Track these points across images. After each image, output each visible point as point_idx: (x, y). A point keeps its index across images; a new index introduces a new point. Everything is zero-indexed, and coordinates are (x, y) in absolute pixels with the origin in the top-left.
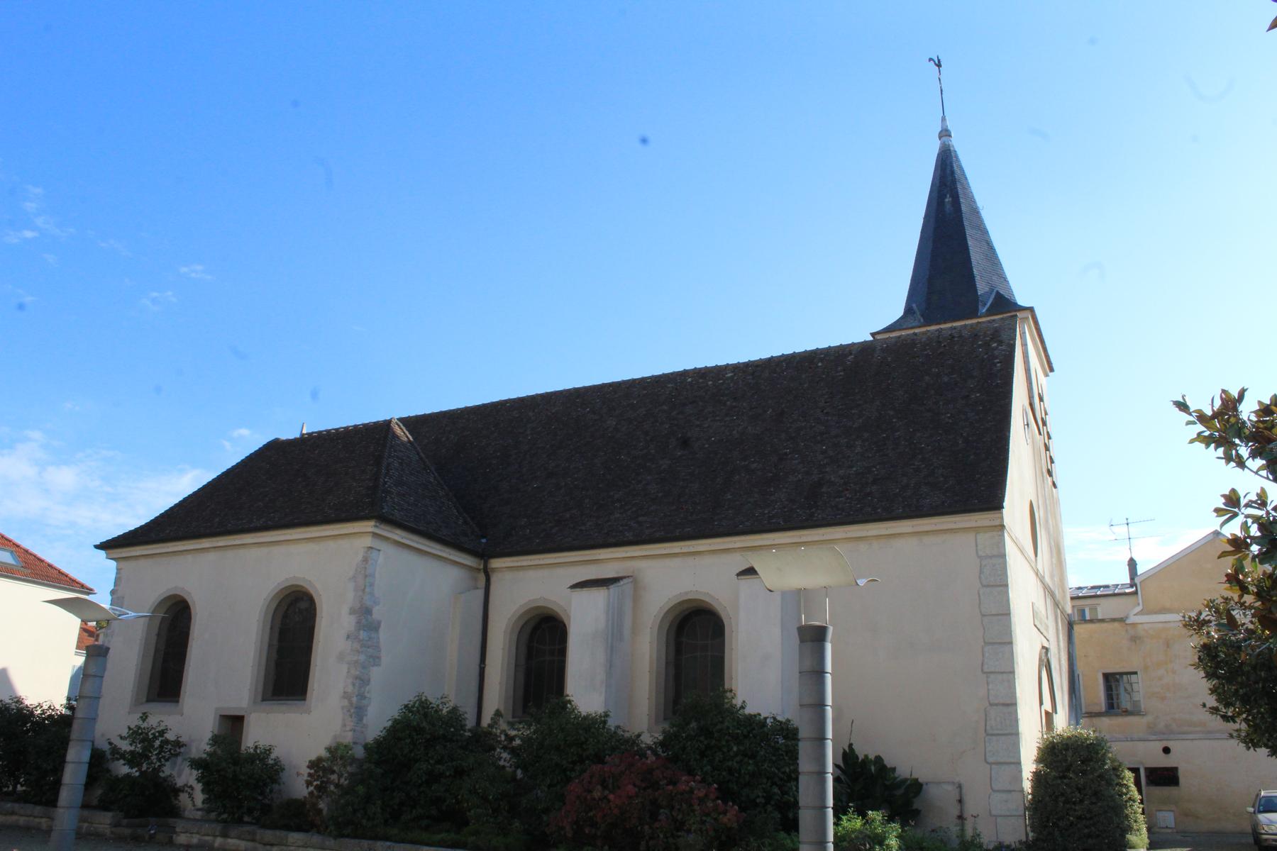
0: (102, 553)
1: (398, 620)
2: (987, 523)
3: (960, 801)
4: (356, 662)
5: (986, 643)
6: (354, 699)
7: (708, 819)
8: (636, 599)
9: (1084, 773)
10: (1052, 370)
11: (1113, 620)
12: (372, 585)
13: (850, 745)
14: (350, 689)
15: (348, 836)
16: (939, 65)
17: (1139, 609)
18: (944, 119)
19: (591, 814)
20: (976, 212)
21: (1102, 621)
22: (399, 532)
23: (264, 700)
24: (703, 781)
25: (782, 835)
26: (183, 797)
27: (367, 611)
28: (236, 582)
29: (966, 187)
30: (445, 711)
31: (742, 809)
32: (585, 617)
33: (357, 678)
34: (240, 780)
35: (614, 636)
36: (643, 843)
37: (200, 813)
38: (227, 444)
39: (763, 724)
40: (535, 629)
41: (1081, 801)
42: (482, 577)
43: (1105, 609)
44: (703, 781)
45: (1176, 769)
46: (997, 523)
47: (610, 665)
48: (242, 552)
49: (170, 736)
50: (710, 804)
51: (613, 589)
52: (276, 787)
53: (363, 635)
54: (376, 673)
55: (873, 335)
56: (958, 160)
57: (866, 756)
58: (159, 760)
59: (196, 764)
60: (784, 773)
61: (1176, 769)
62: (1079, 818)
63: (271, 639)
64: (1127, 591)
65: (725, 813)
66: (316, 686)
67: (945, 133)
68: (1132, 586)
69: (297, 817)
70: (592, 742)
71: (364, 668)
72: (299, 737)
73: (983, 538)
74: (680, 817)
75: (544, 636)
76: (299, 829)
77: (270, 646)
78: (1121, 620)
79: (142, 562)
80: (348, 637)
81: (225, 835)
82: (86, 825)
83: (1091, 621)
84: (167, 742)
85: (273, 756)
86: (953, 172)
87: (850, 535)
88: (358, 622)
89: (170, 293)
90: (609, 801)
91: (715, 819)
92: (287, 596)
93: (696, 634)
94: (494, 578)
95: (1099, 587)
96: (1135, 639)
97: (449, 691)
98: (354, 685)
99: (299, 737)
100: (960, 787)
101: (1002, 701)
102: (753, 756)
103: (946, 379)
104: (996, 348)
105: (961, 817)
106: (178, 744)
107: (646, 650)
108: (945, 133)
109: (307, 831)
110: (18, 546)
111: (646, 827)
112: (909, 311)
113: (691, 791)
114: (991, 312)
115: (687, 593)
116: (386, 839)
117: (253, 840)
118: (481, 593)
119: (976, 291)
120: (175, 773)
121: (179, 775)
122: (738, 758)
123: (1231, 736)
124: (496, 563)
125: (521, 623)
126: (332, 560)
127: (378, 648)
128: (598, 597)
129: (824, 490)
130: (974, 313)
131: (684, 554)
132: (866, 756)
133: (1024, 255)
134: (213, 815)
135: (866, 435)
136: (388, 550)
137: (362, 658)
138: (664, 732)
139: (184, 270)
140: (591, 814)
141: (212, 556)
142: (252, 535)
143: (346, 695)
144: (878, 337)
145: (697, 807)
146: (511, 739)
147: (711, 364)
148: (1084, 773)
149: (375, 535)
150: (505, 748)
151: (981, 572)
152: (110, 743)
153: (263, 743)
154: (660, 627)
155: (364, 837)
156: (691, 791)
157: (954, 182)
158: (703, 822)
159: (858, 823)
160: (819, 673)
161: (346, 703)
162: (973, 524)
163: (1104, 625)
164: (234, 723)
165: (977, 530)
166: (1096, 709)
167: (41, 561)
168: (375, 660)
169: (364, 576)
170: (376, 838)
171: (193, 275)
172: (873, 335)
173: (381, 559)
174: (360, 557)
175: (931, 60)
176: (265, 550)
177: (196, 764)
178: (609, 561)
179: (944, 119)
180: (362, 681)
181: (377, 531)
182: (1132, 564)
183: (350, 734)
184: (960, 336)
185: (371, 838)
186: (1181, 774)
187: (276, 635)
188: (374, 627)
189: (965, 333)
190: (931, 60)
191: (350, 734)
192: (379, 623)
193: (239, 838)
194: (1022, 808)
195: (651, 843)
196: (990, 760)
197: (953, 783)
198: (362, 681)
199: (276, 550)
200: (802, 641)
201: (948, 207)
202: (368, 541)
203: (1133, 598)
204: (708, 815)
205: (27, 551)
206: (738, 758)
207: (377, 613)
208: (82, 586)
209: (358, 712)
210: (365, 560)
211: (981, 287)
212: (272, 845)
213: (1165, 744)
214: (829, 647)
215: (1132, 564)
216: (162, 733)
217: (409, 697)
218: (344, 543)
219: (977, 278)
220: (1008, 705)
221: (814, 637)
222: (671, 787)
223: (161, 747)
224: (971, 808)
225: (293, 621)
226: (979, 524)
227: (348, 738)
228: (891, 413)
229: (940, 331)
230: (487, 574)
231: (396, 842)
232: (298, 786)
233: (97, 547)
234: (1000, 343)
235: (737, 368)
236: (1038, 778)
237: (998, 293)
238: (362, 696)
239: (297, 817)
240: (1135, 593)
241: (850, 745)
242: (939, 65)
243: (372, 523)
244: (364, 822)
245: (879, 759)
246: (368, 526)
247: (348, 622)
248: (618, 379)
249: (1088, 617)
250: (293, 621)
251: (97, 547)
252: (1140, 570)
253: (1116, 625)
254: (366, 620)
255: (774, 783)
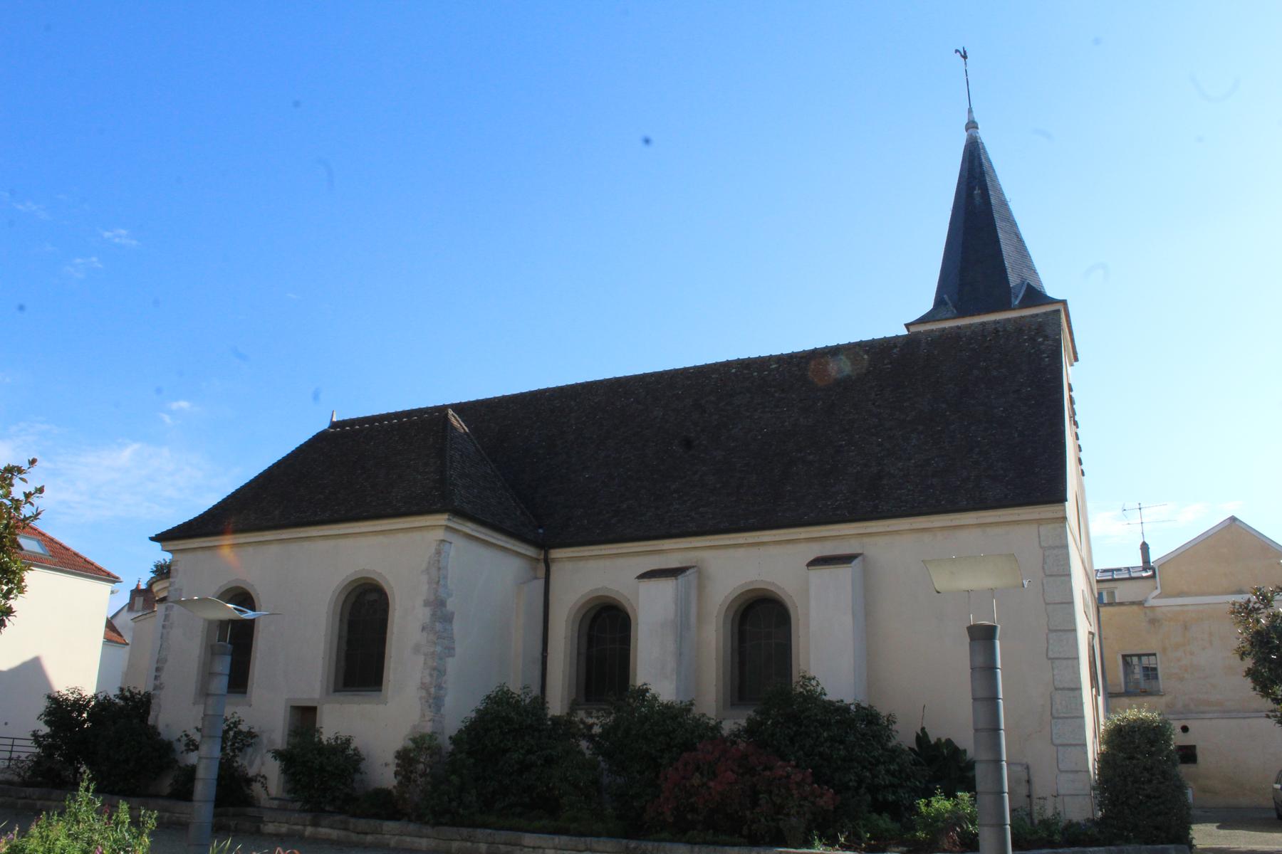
0: (158, 545)
1: (466, 608)
2: (1050, 515)
3: (1028, 781)
4: (433, 653)
5: (1051, 631)
6: (432, 690)
7: (806, 803)
8: (701, 588)
9: (1151, 754)
10: (1076, 359)
11: (1133, 603)
12: (445, 577)
13: (923, 729)
14: (427, 680)
15: (446, 824)
16: (965, 57)
17: (1158, 591)
18: (970, 111)
19: (692, 800)
20: (1004, 204)
21: (1121, 604)
22: (469, 524)
23: (336, 691)
24: (797, 766)
25: (875, 816)
26: (257, 787)
27: (442, 603)
28: (303, 574)
29: (995, 179)
30: (528, 701)
31: (836, 793)
32: (652, 609)
33: (434, 669)
34: (322, 773)
35: (683, 626)
36: (745, 827)
37: (276, 802)
38: (167, 419)
39: (846, 709)
40: (594, 619)
41: (1150, 781)
42: (542, 565)
43: (1123, 592)
44: (797, 766)
45: (1194, 747)
46: (1059, 515)
47: (680, 655)
48: (306, 544)
49: (243, 727)
50: (808, 788)
51: (681, 578)
52: (357, 777)
53: (438, 626)
54: (451, 664)
55: (907, 326)
56: (985, 152)
57: (939, 739)
58: (233, 751)
59: (278, 755)
60: (874, 757)
61: (1194, 747)
62: (1148, 796)
63: (340, 630)
64: (1144, 574)
65: (821, 796)
66: (391, 677)
67: (972, 125)
68: (1145, 569)
69: (384, 806)
70: (672, 730)
71: (441, 659)
72: (380, 728)
73: (1045, 529)
74: (779, 801)
75: (607, 626)
76: (391, 817)
77: (340, 638)
78: (1140, 603)
79: (200, 554)
80: (423, 629)
81: (315, 824)
82: (167, 815)
83: (1110, 604)
84: (240, 732)
85: (352, 746)
86: (981, 164)
87: (915, 526)
88: (434, 615)
89: (94, 259)
90: (709, 788)
91: (813, 803)
92: (354, 590)
93: (761, 623)
94: (554, 568)
95: (1112, 570)
96: (1153, 621)
97: (518, 681)
98: (431, 675)
99: (380, 728)
100: (1028, 768)
101: (1066, 685)
102: (842, 742)
103: (995, 373)
104: (1041, 343)
105: (1029, 796)
106: (251, 734)
107: (713, 638)
108: (972, 125)
109: (399, 820)
110: (44, 535)
111: (748, 813)
112: (939, 302)
113: (788, 777)
114: (1025, 304)
115: (752, 582)
116: (485, 826)
117: (345, 829)
118: (542, 582)
119: (1007, 282)
120: (246, 763)
121: (251, 763)
122: (828, 744)
123: (1268, 717)
124: (556, 553)
125: (343, 597)
126: (410, 555)
127: (452, 639)
128: (666, 587)
129: (885, 482)
130: (1007, 306)
131: (741, 545)
132: (939, 739)
133: (1055, 251)
134: (298, 805)
135: (921, 428)
136: (459, 542)
137: (439, 649)
138: (748, 719)
139: (107, 234)
140: (692, 800)
141: (275, 548)
142: (319, 528)
143: (424, 686)
144: (913, 329)
145: (795, 792)
146: (591, 727)
147: (754, 355)
148: (1151, 754)
149: (447, 528)
150: (584, 736)
151: (1044, 562)
152: (187, 736)
153: (344, 734)
154: (726, 616)
155: (462, 825)
156: (788, 777)
157: (982, 174)
158: (801, 806)
159: (948, 805)
160: (991, 668)
161: (424, 693)
162: (1036, 516)
163: (1123, 608)
164: (305, 716)
165: (1039, 522)
166: (1117, 690)
167: (68, 549)
168: (450, 651)
169: (437, 569)
170: (475, 825)
171: (117, 240)
172: (907, 326)
173: (452, 553)
174: (433, 550)
175: (957, 51)
176: (331, 543)
177: (278, 755)
178: (673, 551)
179: (970, 111)
180: (439, 672)
181: (451, 524)
182: (1145, 548)
183: (430, 724)
184: (1005, 330)
185: (469, 826)
186: (1199, 752)
187: (345, 627)
188: (448, 619)
189: (1010, 328)
190: (957, 51)
191: (430, 724)
192: (453, 614)
193: (331, 827)
194: (1088, 788)
195: (754, 826)
196: (1058, 742)
197: (1022, 765)
198: (439, 672)
199: (343, 543)
200: (972, 639)
201: (978, 200)
202: (441, 534)
203: (1151, 582)
204: (805, 799)
205: (52, 540)
206: (828, 744)
207: (451, 605)
208: (108, 574)
209: (435, 701)
210: (438, 553)
211: (1013, 280)
212: (366, 834)
213: (1184, 723)
214: (998, 643)
215: (1145, 548)
216: (236, 724)
217: (492, 688)
218: (417, 536)
219: (1009, 271)
220: (1072, 689)
221: (983, 636)
222: (768, 773)
223: (235, 737)
224: (1038, 791)
225: (364, 614)
226: (1043, 516)
227: (428, 728)
228: (944, 406)
229: (983, 324)
230: (547, 563)
231: (496, 829)
232: (384, 774)
233: (152, 539)
234: (1046, 337)
235: (780, 359)
236: (1105, 761)
237: (1029, 285)
238: (439, 687)
239: (384, 806)
240: (1153, 576)
241: (923, 729)
242: (965, 57)
243: (446, 516)
244: (461, 811)
245: (949, 742)
246: (442, 519)
247: (423, 614)
248: (660, 369)
249: (1105, 601)
250: (364, 614)
251: (152, 539)
252: (1154, 556)
253: (1135, 608)
254: (440, 612)
255: (864, 767)
